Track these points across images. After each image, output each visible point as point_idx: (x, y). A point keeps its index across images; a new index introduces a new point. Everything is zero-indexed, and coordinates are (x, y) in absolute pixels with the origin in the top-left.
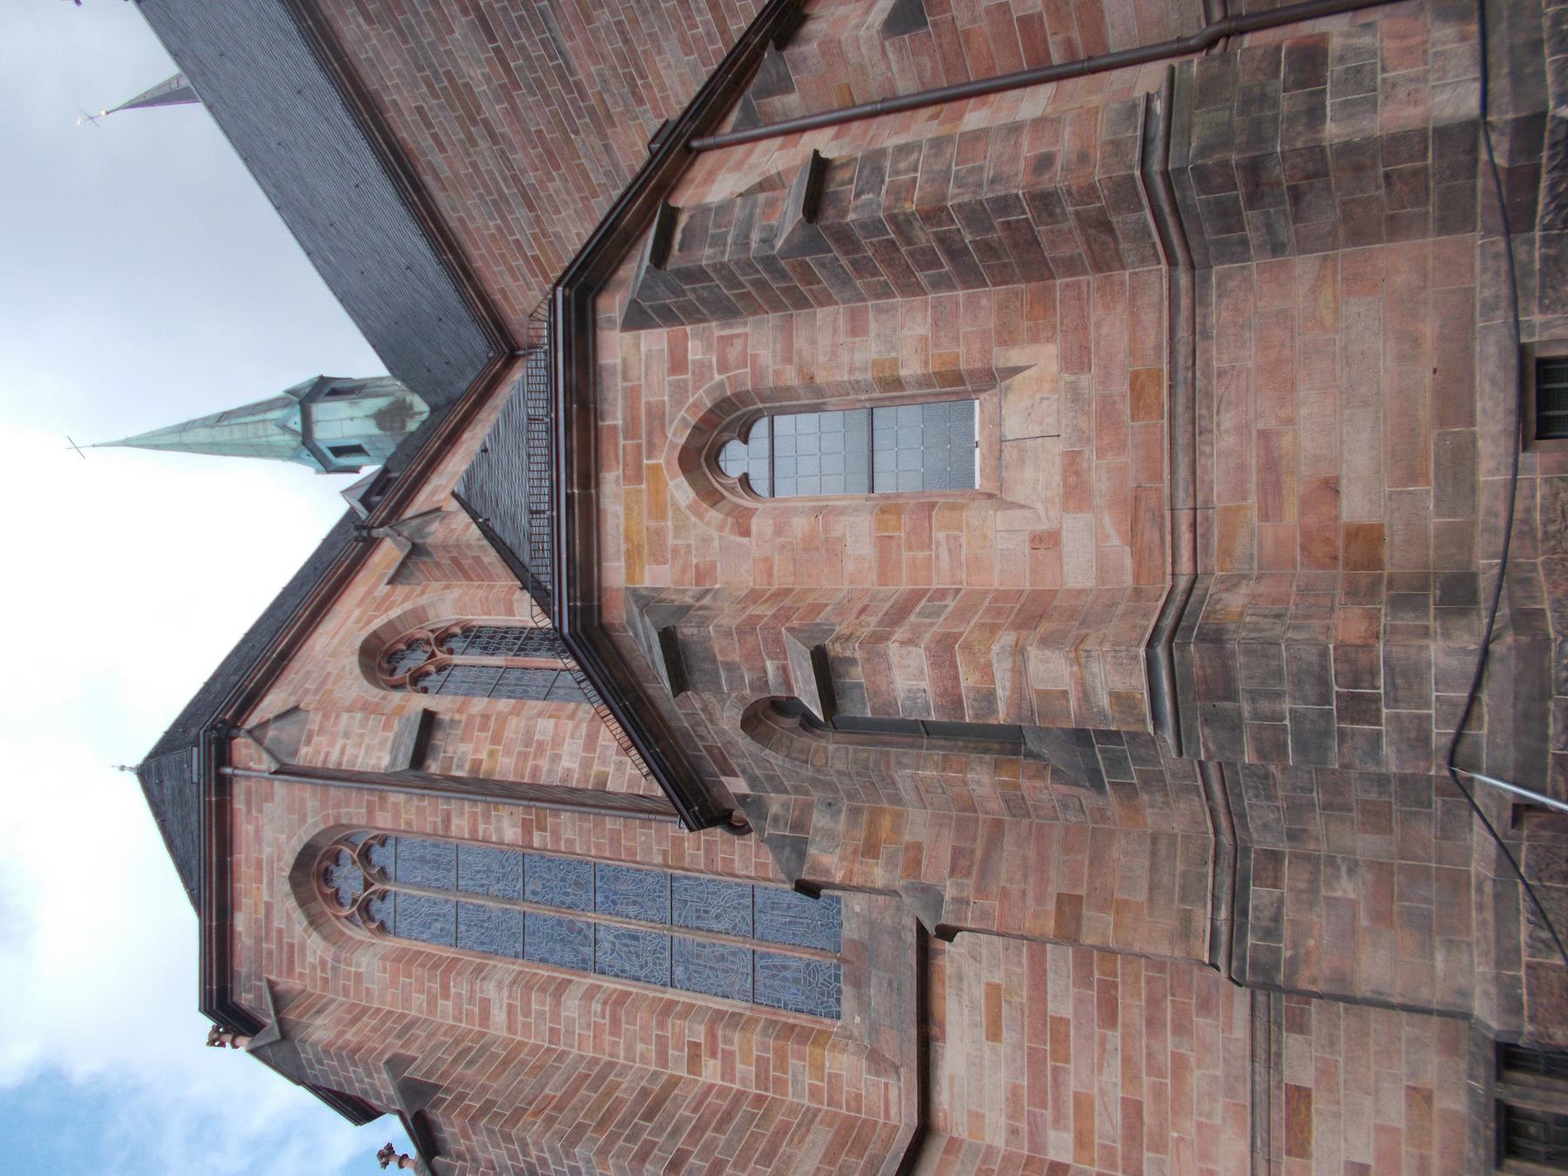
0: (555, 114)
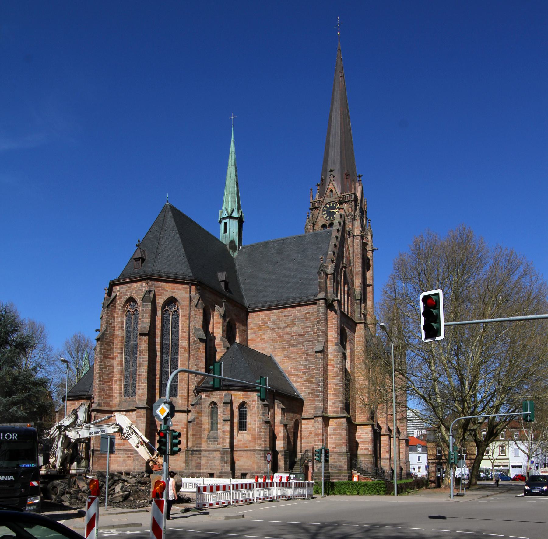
0: (286, 341)
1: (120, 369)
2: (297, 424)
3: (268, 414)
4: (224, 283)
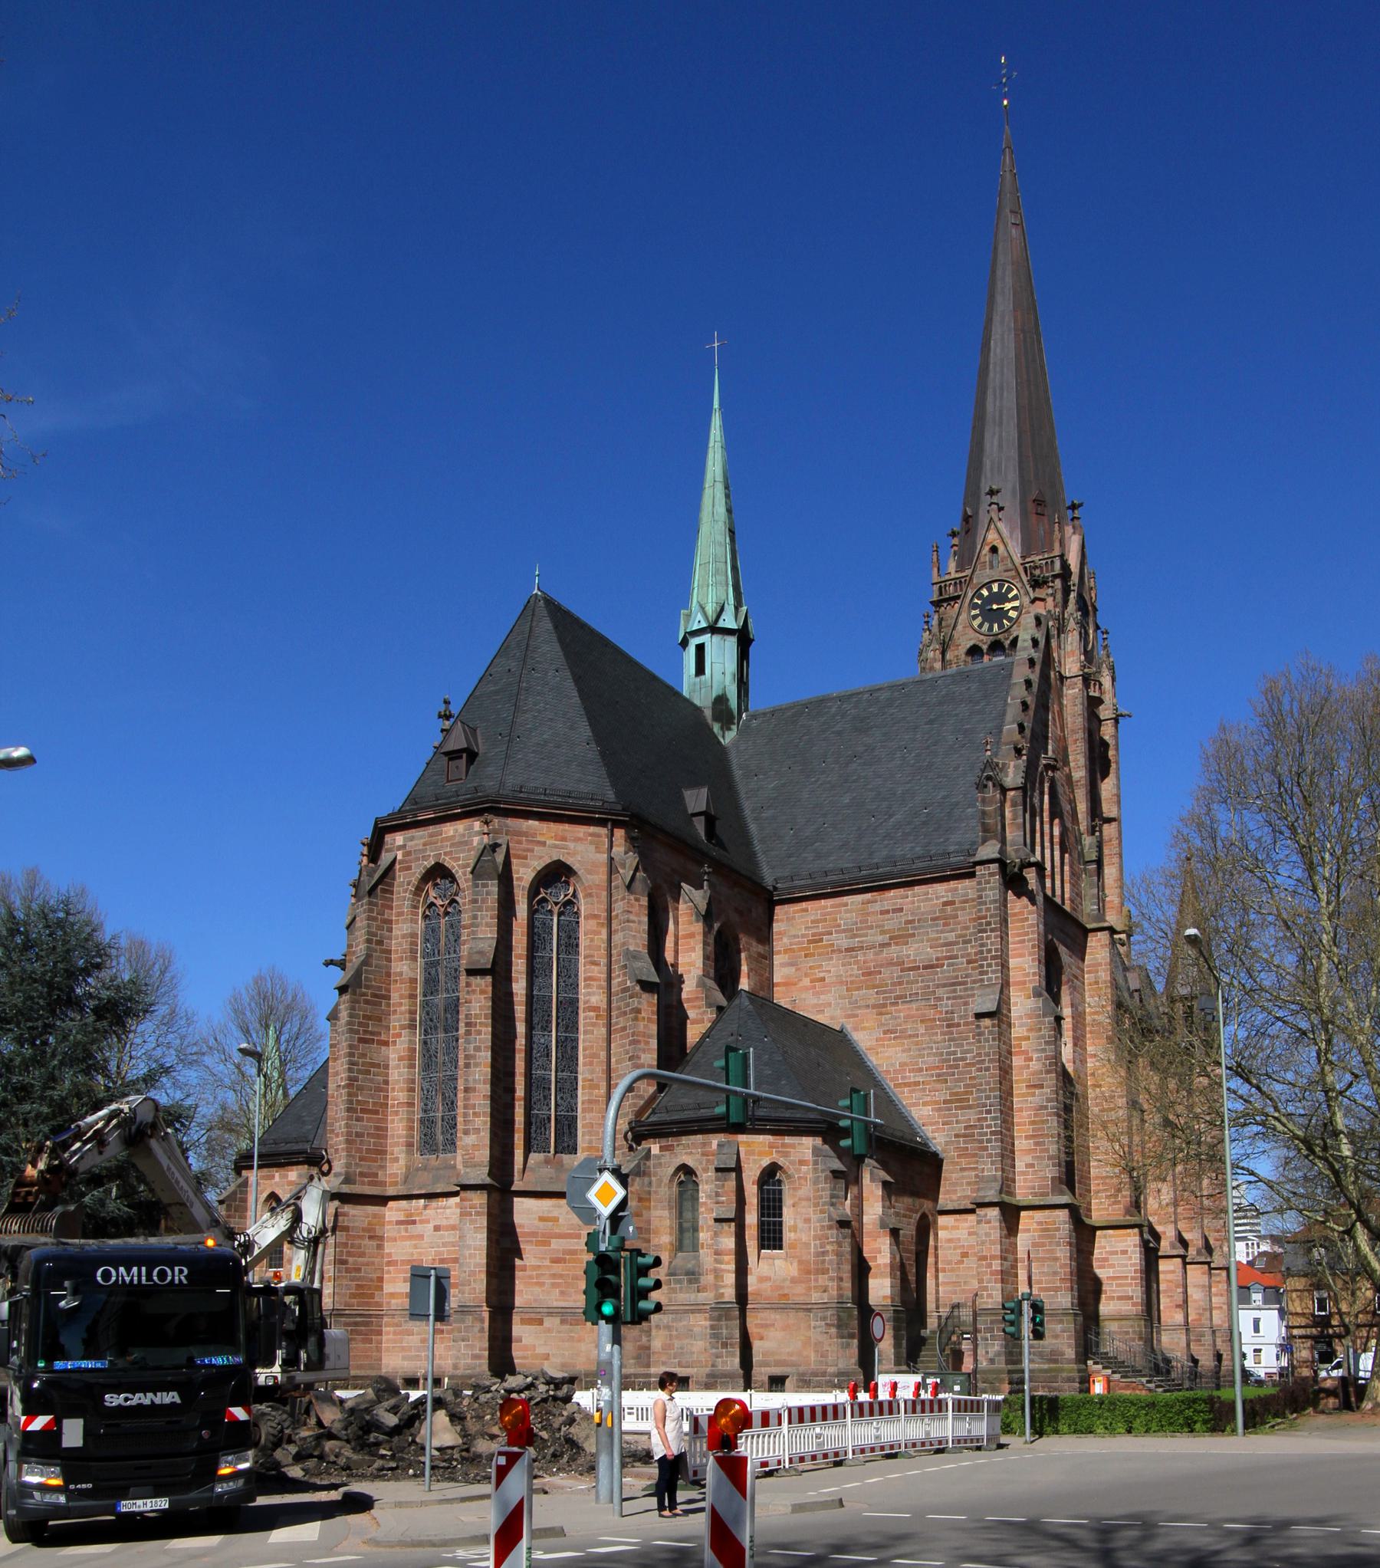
0: (887, 985)
1: (409, 1073)
2: (925, 1229)
3: (846, 1199)
4: (702, 818)
